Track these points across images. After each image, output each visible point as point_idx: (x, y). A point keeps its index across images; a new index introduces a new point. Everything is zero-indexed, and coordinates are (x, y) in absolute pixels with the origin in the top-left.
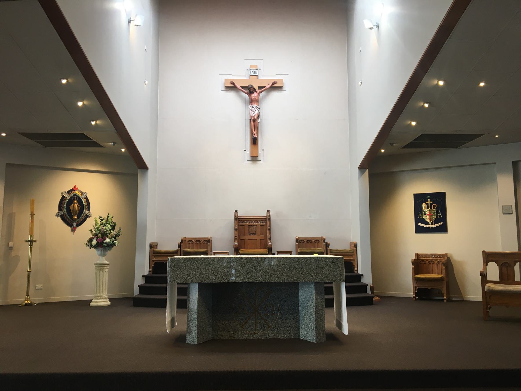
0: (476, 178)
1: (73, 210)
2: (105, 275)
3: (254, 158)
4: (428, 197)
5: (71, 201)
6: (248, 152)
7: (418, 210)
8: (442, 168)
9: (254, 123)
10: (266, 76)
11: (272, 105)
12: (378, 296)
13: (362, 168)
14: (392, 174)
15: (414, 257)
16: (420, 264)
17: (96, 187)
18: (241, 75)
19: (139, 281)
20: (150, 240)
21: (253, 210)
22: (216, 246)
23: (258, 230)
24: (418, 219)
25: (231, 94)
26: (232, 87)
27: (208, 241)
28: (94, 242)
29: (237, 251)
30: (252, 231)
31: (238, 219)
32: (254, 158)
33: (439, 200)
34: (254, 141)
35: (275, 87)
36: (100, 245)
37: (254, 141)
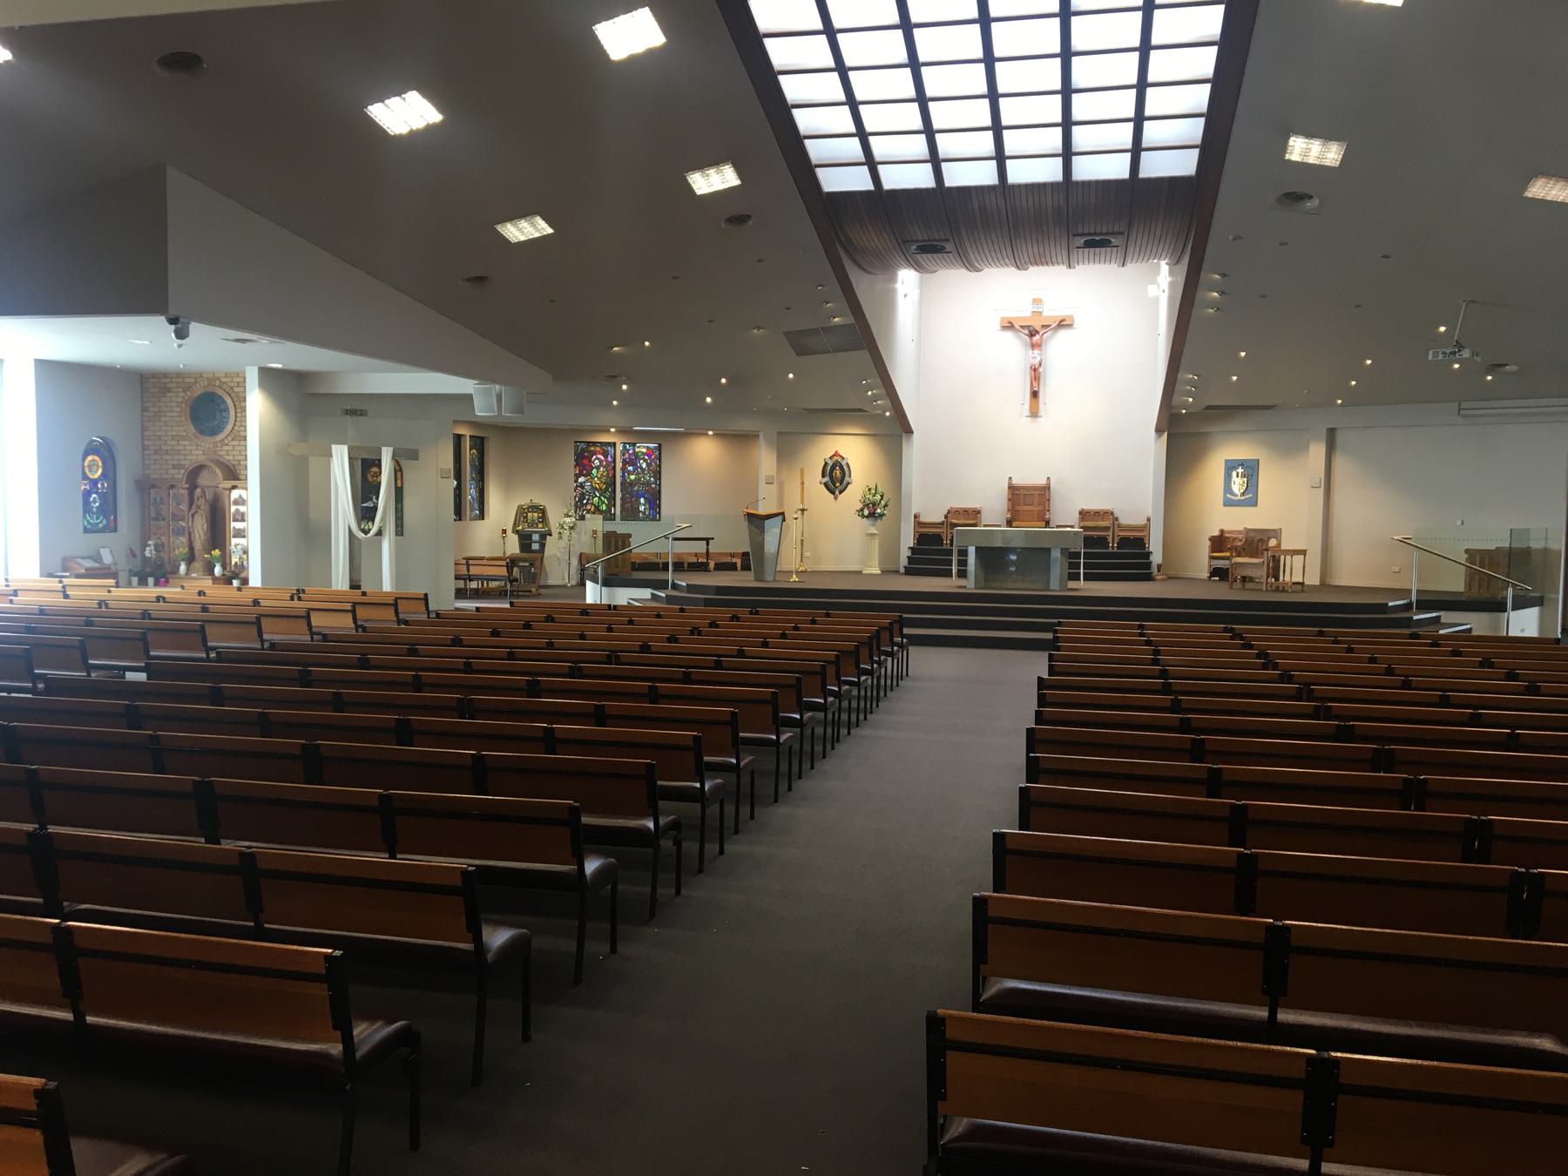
0: (1291, 448)
1: (836, 476)
2: (876, 544)
3: (1034, 413)
4: (1014, 558)
5: (833, 468)
6: (1027, 406)
7: (1228, 477)
8: (201, 966)
9: (1036, 373)
10: (1052, 310)
11: (1058, 347)
12: (145, 546)
13: (1159, 430)
14: (1202, 436)
15: (1217, 533)
16: (1219, 542)
17: (854, 448)
18: (1021, 310)
19: (905, 553)
20: (914, 511)
21: (1029, 477)
22: (987, 518)
23: (1036, 500)
24: (1228, 488)
25: (1009, 335)
26: (1009, 326)
27: (977, 512)
28: (866, 512)
29: (1009, 523)
30: (1028, 501)
31: (1012, 488)
32: (1034, 413)
33: (1251, 470)
34: (1035, 394)
35: (1063, 324)
36: (872, 515)
37: (1035, 394)
